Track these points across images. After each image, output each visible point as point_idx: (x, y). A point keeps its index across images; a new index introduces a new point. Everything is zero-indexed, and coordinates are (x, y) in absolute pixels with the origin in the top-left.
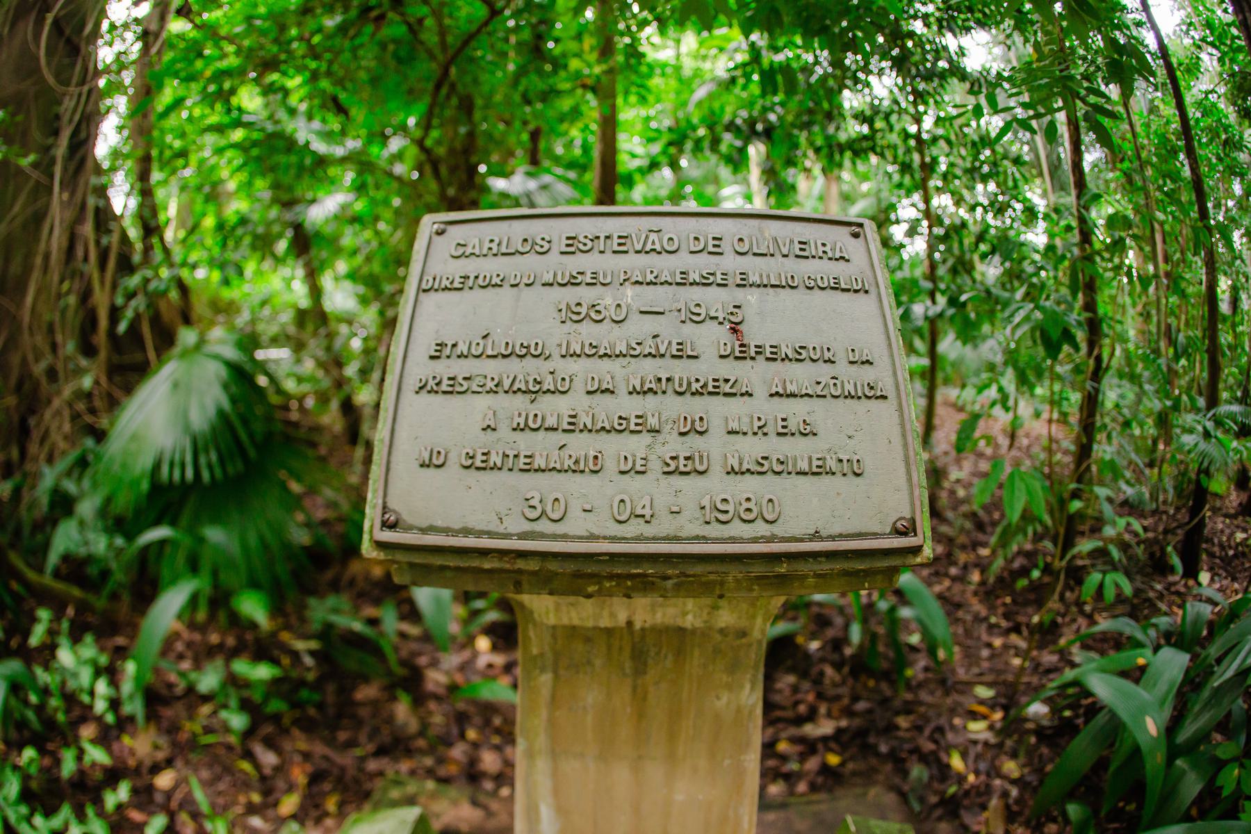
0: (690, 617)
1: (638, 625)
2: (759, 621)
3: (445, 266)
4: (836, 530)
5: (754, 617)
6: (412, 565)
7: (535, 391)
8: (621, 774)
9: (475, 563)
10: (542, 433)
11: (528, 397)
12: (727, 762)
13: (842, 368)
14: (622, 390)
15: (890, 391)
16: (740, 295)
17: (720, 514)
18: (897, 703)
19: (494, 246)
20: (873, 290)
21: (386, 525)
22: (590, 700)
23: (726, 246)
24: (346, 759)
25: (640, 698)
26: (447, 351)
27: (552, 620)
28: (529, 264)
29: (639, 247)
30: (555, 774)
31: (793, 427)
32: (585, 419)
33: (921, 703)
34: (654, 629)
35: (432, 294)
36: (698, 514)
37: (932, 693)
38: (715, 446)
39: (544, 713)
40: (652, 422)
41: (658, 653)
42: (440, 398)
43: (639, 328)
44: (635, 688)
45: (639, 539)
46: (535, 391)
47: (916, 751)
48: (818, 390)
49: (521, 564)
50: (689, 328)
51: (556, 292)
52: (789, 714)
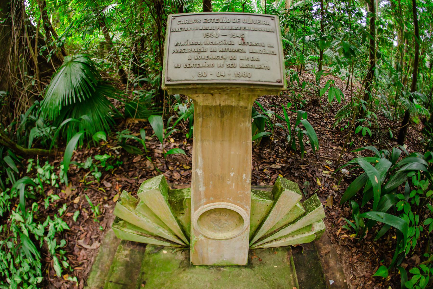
0: (234, 103)
1: (222, 105)
2: (250, 105)
3: (176, 26)
4: (264, 80)
5: (248, 104)
6: (173, 89)
7: (199, 52)
8: (218, 145)
9: (188, 87)
10: (201, 60)
11: (198, 53)
12: (244, 143)
13: (266, 48)
14: (218, 51)
15: (277, 53)
16: (244, 32)
17: (239, 76)
18: (301, 161)
19: (188, 21)
20: (275, 32)
21: (168, 81)
22: (211, 125)
23: (241, 21)
24: (133, 181)
25: (222, 124)
26: (179, 44)
27: (202, 104)
28: (196, 25)
29: (221, 21)
30: (202, 147)
31: (254, 59)
32: (210, 57)
33: (308, 162)
34: (225, 106)
35: (174, 33)
36: (234, 75)
37: (312, 159)
38: (237, 62)
39: (200, 129)
40: (224, 57)
41: (226, 112)
42: (178, 54)
43: (221, 39)
44: (221, 121)
45: (222, 80)
46: (199, 52)
47: (306, 176)
48: (261, 52)
49: (198, 86)
50: (232, 39)
51: (203, 31)
52: (268, 161)
